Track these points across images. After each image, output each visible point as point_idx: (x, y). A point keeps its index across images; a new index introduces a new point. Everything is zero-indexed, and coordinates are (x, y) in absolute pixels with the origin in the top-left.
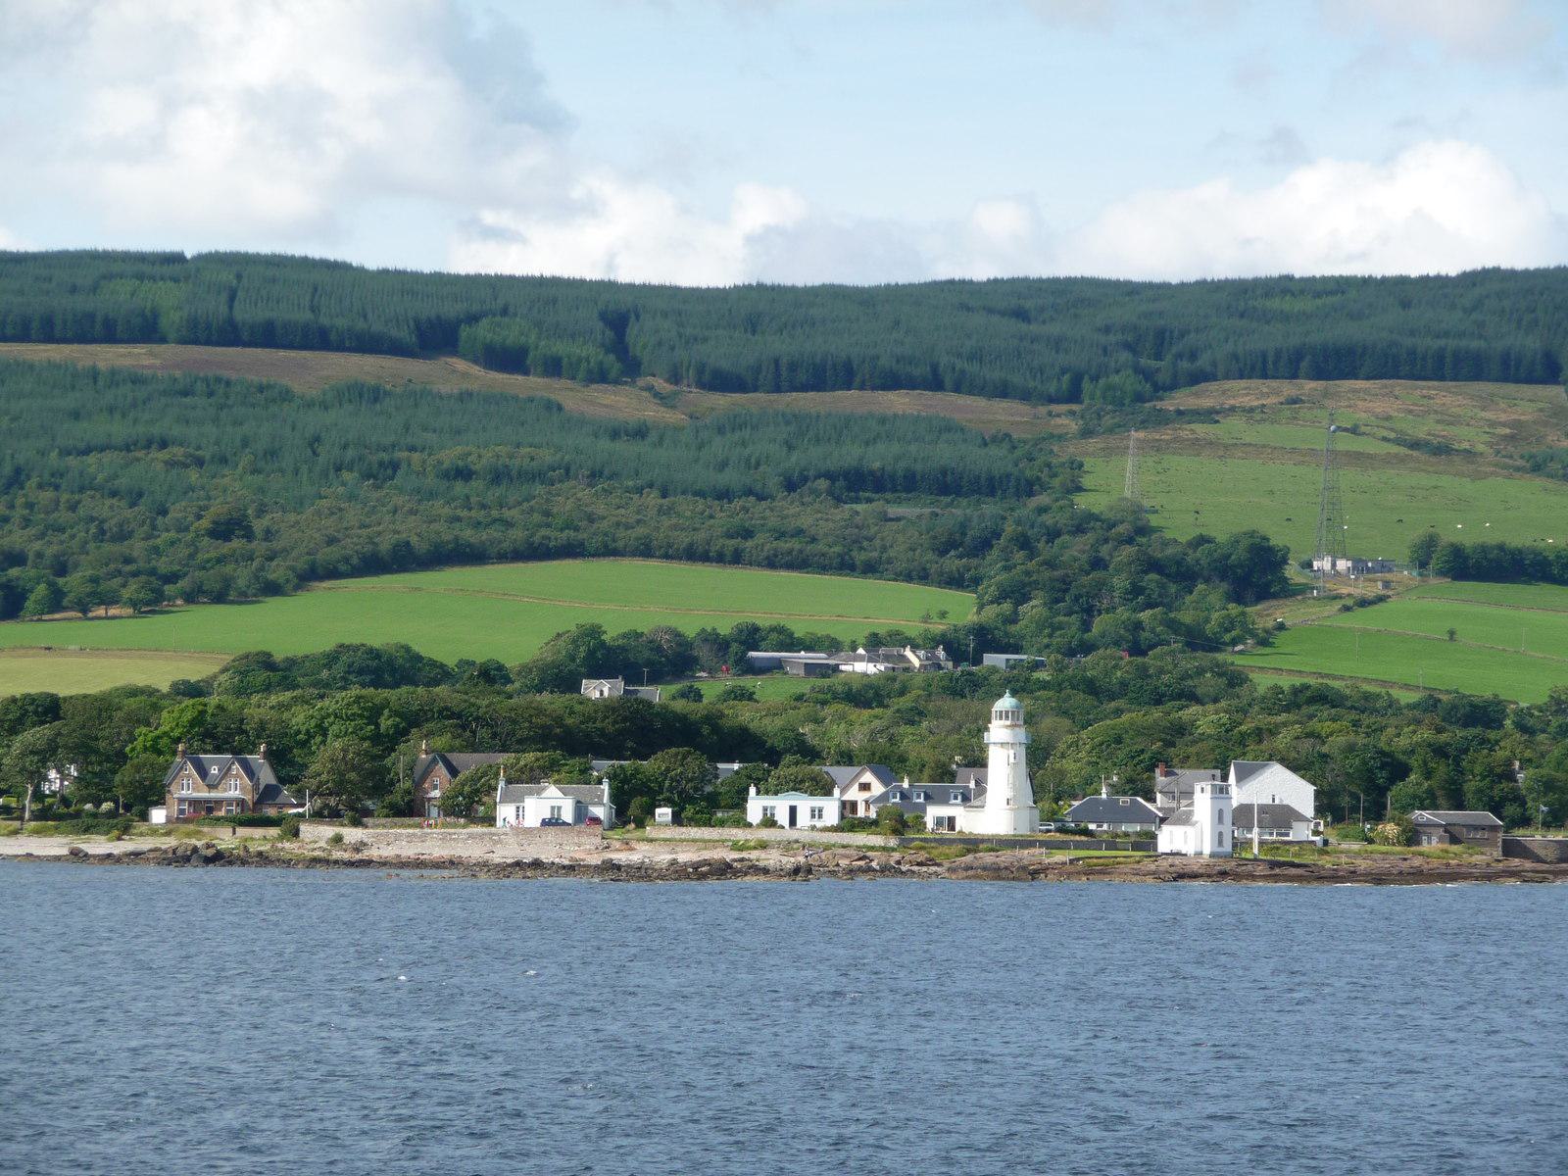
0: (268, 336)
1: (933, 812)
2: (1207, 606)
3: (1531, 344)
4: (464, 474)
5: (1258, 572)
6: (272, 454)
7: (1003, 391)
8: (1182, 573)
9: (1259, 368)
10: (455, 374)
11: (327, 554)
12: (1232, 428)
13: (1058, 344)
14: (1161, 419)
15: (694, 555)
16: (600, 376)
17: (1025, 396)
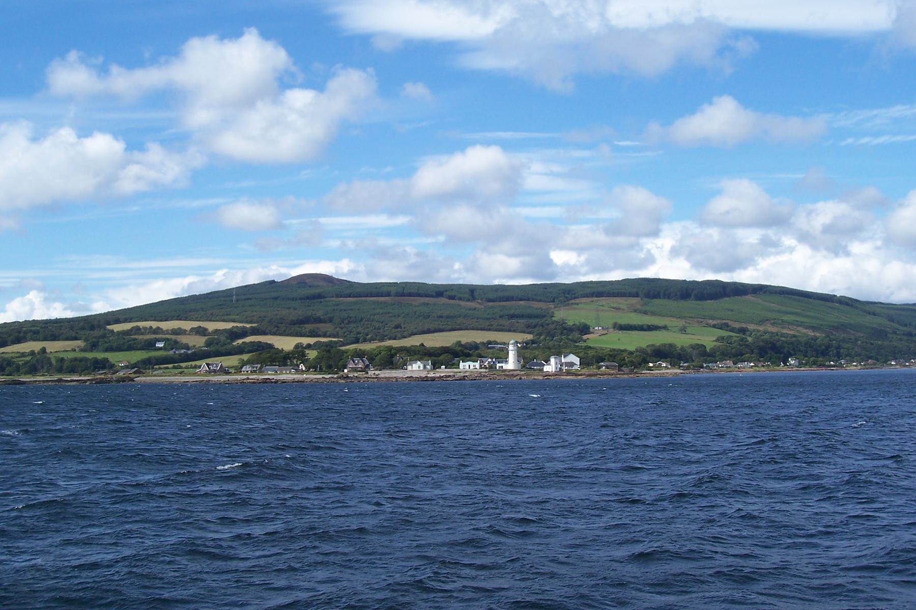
0: (410, 295)
1: (498, 365)
2: (576, 335)
3: (634, 290)
4: (441, 317)
5: (585, 329)
6: (408, 315)
7: (540, 301)
8: (570, 330)
9: (587, 296)
10: (443, 300)
11: (415, 331)
12: (580, 306)
13: (551, 293)
14: (569, 305)
15: (482, 329)
16: (468, 300)
17: (545, 301)
